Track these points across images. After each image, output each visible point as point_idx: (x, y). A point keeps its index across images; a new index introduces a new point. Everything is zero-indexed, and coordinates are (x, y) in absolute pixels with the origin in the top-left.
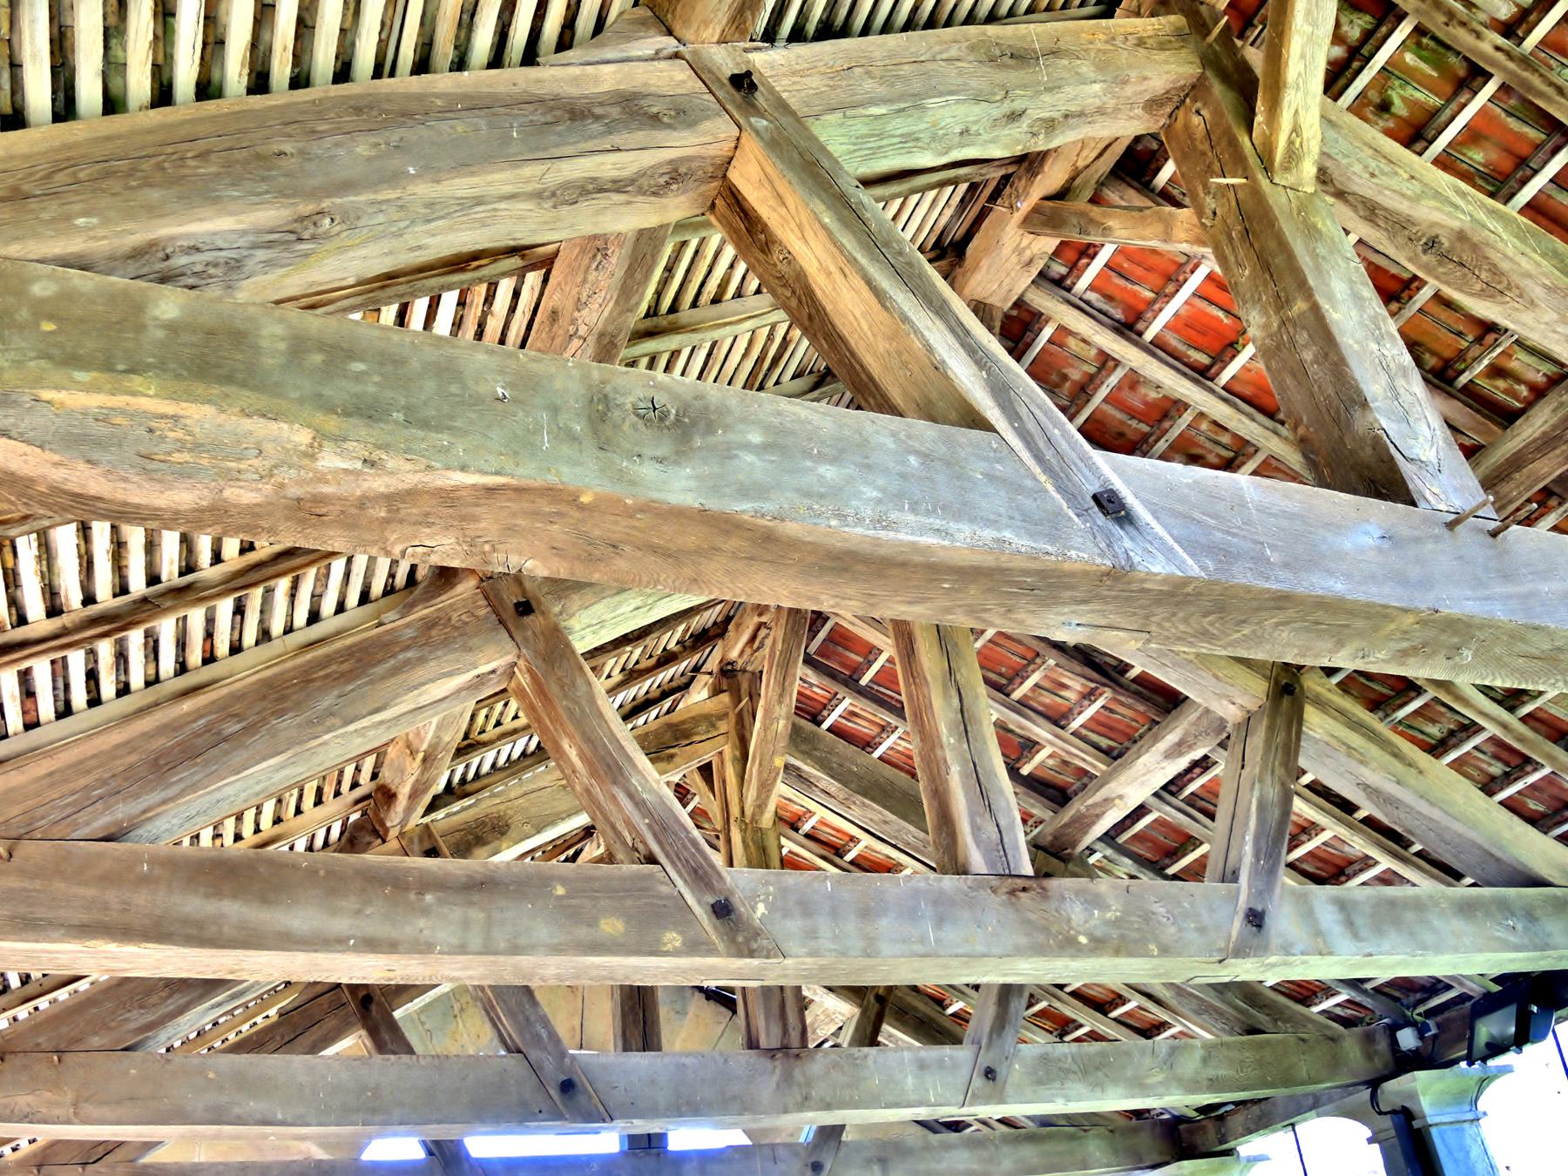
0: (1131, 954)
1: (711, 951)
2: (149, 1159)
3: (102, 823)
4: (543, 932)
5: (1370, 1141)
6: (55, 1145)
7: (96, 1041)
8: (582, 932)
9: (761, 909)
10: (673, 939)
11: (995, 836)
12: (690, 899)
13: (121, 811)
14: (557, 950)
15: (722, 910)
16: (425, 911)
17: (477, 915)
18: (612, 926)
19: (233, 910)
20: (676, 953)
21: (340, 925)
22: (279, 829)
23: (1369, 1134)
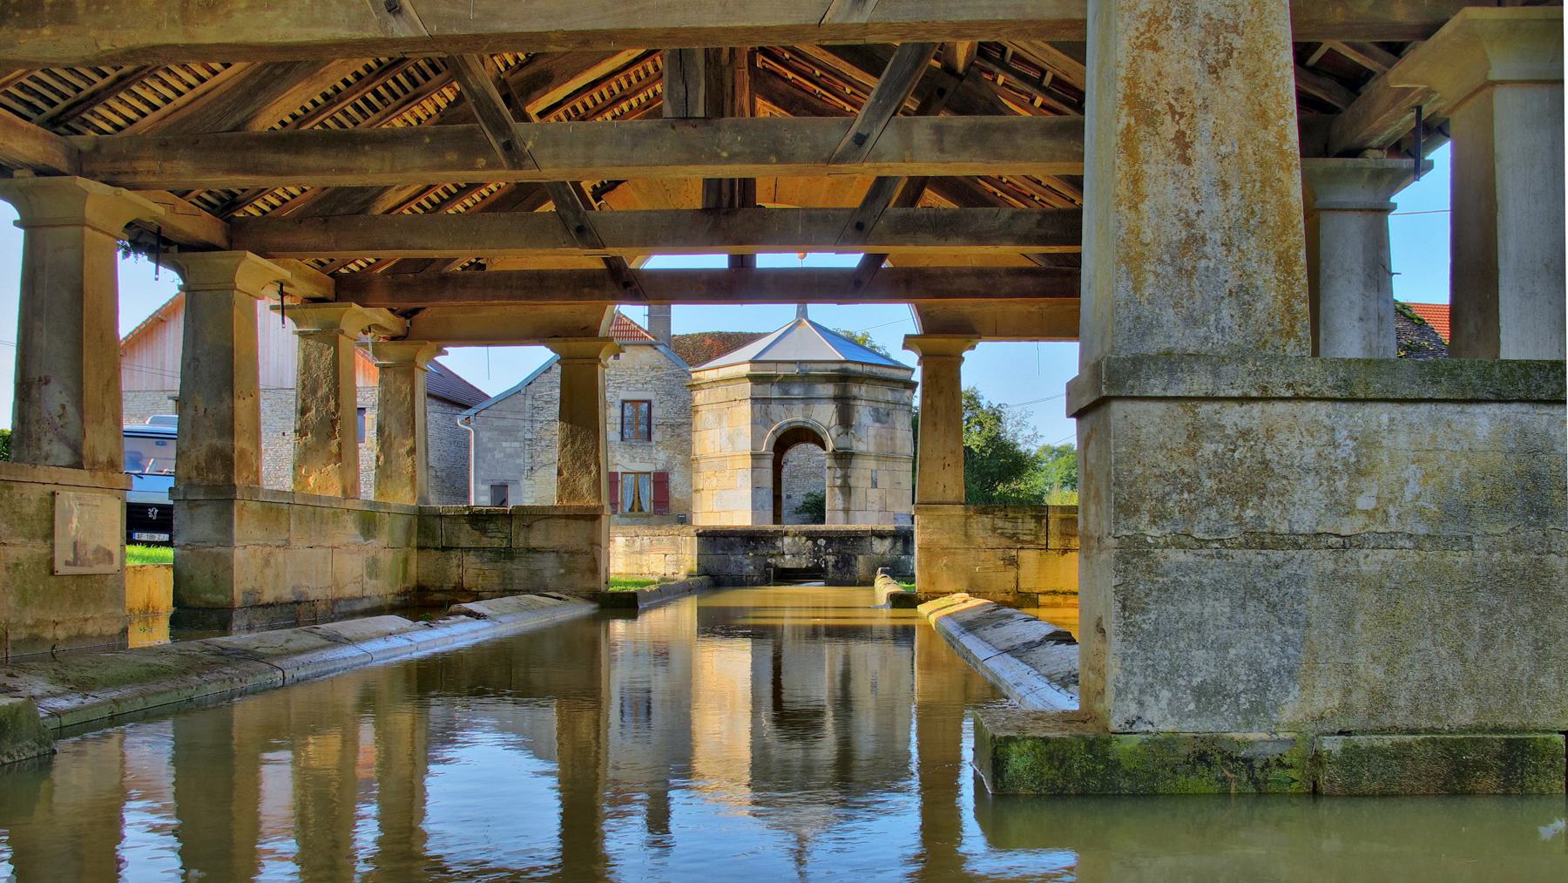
0: (1304, 128)
1: (500, 167)
2: (446, 270)
3: (230, 123)
4: (418, 161)
5: (16, 223)
6: (404, 261)
7: (342, 210)
8: (436, 160)
9: (530, 144)
10: (481, 162)
11: (682, 94)
12: (492, 140)
13: (238, 117)
14: (424, 169)
15: (508, 147)
16: (365, 154)
17: (388, 155)
18: (452, 157)
19: (285, 159)
20: (483, 169)
21: (327, 163)
22: (418, 90)
23: (18, 217)
